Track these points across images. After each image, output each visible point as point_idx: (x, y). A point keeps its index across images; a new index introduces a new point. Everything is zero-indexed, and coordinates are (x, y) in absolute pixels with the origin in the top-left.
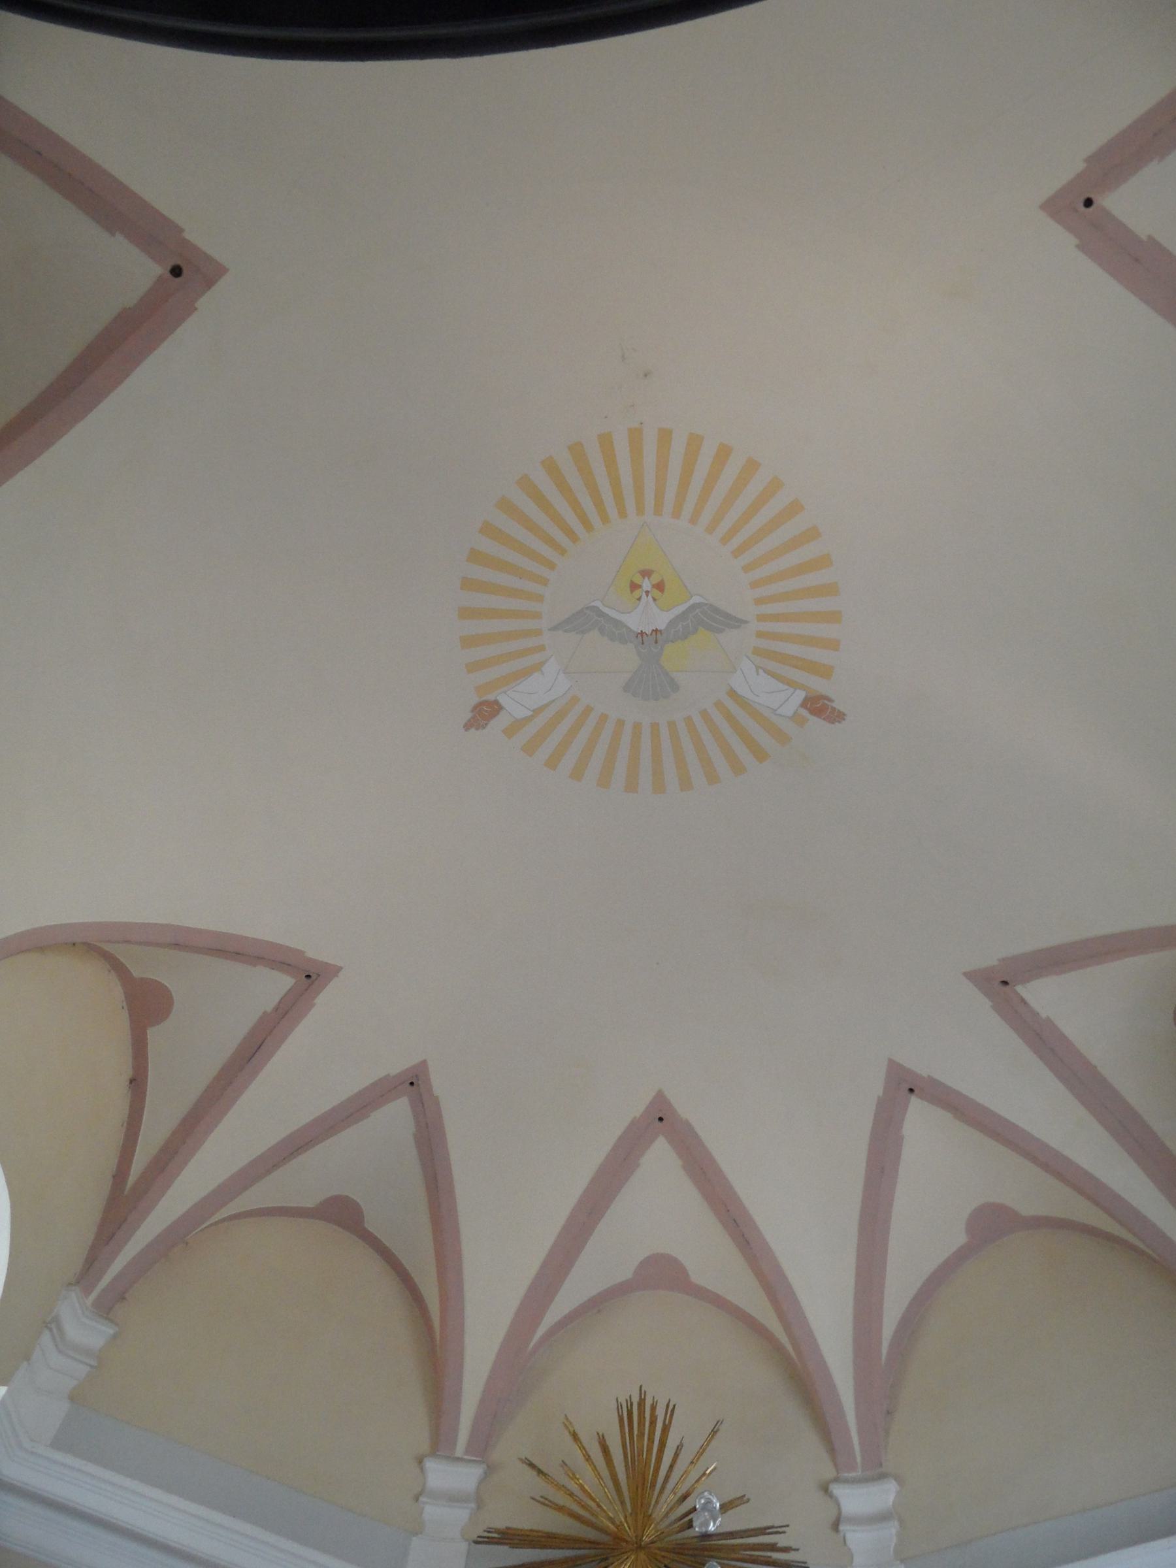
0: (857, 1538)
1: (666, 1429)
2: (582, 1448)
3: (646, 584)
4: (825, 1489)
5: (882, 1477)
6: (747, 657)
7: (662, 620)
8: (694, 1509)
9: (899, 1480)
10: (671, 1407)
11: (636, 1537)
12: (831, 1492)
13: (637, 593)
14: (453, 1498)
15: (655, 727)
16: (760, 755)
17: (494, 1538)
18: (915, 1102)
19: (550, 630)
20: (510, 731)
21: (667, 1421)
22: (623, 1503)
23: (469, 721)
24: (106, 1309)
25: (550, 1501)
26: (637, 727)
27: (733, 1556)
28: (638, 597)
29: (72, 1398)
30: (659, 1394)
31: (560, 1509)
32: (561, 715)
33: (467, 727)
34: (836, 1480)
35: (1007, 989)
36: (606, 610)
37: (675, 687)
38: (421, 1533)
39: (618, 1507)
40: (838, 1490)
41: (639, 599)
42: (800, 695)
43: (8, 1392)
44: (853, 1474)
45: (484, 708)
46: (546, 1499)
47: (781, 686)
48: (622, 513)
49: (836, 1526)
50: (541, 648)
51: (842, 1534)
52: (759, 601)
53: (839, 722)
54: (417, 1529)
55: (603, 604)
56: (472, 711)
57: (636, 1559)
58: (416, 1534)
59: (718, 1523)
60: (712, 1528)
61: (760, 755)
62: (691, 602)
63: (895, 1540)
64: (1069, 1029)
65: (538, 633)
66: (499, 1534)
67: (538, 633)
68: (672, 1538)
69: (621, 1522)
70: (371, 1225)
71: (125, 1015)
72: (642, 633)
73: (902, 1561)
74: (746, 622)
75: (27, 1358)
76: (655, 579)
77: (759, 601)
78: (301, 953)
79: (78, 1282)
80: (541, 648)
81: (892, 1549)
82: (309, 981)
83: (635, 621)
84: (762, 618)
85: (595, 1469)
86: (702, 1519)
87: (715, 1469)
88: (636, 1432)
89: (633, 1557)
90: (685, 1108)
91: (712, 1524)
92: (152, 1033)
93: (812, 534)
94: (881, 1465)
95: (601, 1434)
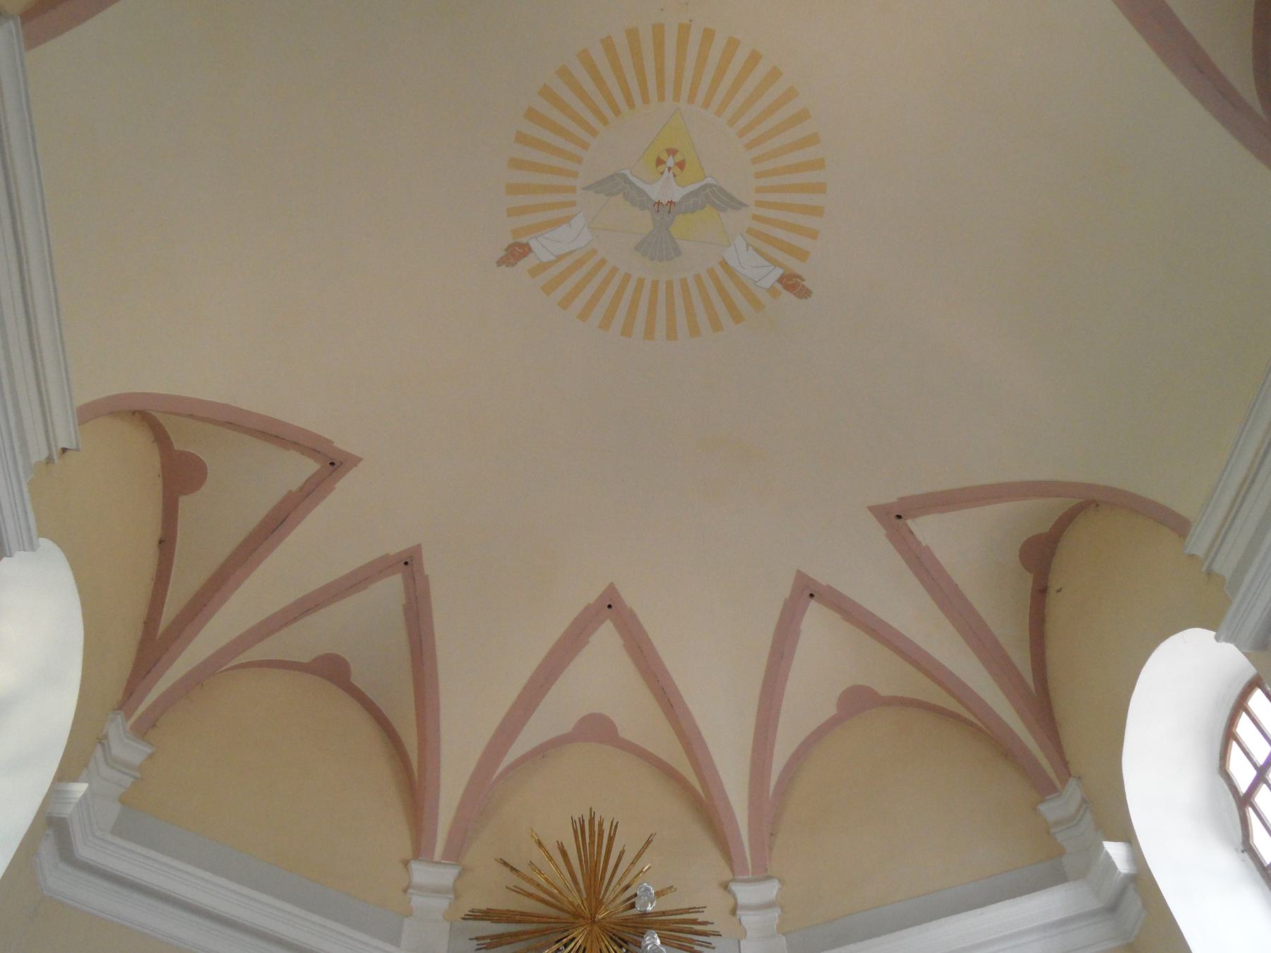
0: (749, 920)
1: (611, 839)
2: (546, 852)
3: (670, 162)
4: (726, 886)
5: (768, 878)
6: (741, 234)
7: (677, 194)
8: (636, 895)
9: (782, 882)
10: (614, 824)
11: (591, 915)
12: (731, 889)
13: (661, 168)
14: (437, 891)
15: (655, 284)
16: (737, 317)
17: (478, 916)
18: (813, 604)
19: (583, 189)
20: (534, 272)
21: (612, 833)
22: (579, 891)
23: (502, 258)
24: (144, 729)
25: (522, 890)
26: (641, 282)
27: (665, 927)
28: (661, 171)
29: (123, 800)
30: (606, 815)
31: (530, 895)
32: (580, 263)
33: (500, 263)
34: (734, 880)
35: (900, 522)
36: (634, 180)
37: (677, 252)
38: (411, 915)
39: (576, 894)
40: (735, 887)
41: (662, 173)
42: (778, 272)
43: (89, 788)
44: (745, 877)
45: (517, 248)
46: (519, 888)
47: (766, 263)
48: (661, 98)
49: (733, 912)
50: (573, 204)
51: (738, 917)
52: (759, 190)
53: (806, 298)
54: (409, 913)
55: (631, 173)
56: (506, 250)
57: (591, 931)
58: (407, 916)
59: (654, 905)
60: (649, 908)
61: (737, 317)
62: (705, 182)
63: (777, 921)
64: (942, 556)
65: (573, 190)
66: (480, 912)
67: (573, 190)
68: (618, 915)
69: (578, 904)
70: (357, 679)
71: (159, 481)
72: (659, 203)
73: (783, 934)
74: (746, 206)
75: (86, 765)
76: (679, 158)
77: (759, 190)
78: (330, 442)
79: (120, 708)
80: (573, 204)
81: (775, 927)
82: (332, 467)
83: (655, 192)
84: (760, 204)
85: (557, 867)
86: (642, 901)
87: (649, 868)
88: (588, 841)
89: (589, 929)
90: (631, 597)
91: (650, 905)
92: (184, 502)
93: (812, 140)
94: (766, 870)
95: (560, 843)
